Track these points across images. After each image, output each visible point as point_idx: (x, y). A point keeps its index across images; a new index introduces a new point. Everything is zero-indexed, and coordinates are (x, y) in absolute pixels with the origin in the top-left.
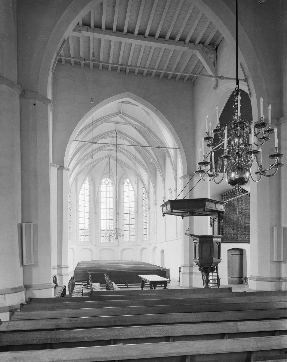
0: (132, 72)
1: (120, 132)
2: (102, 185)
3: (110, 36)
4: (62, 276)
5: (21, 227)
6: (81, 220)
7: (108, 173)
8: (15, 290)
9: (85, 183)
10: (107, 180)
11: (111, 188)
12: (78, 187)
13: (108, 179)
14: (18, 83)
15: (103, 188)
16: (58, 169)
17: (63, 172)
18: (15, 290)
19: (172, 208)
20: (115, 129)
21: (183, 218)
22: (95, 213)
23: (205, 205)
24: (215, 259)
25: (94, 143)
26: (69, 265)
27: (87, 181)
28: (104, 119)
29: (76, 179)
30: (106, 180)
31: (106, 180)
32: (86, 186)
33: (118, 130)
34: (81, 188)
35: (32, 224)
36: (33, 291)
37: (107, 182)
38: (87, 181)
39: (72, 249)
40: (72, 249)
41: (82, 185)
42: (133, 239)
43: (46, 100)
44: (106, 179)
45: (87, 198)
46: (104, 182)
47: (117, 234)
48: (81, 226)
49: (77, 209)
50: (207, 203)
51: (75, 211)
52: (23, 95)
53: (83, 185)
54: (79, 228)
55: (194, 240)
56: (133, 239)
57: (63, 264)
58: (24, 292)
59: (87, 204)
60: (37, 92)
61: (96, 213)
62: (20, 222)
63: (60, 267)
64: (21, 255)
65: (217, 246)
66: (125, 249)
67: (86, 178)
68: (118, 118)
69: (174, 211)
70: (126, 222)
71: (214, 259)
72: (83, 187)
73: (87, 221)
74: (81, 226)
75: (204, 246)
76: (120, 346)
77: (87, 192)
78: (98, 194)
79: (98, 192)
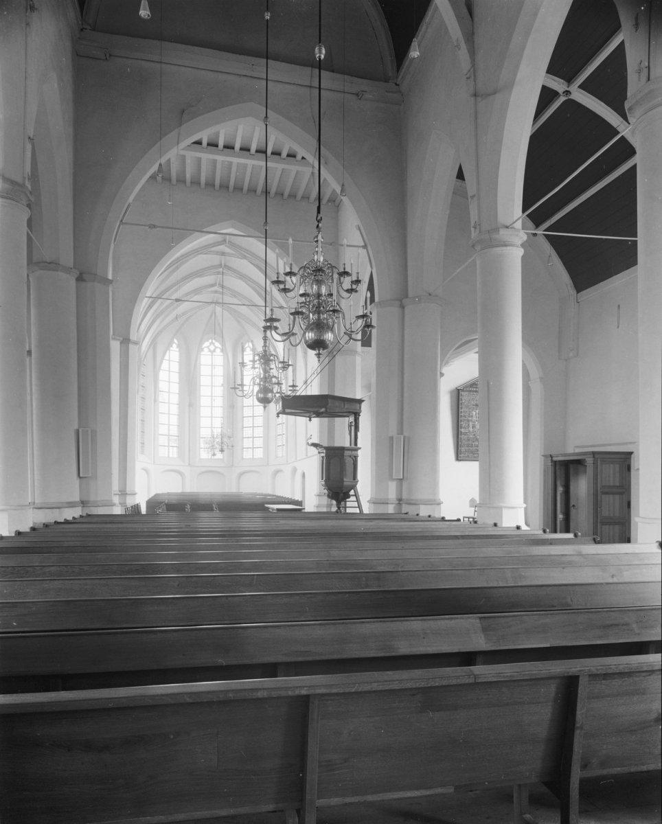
0: (238, 188)
1: (229, 268)
2: (202, 353)
5: (77, 432)
7: (215, 331)
8: (71, 505)
9: (171, 348)
10: (214, 344)
11: (219, 359)
12: (158, 359)
13: (214, 341)
14: (75, 268)
16: (121, 343)
18: (71, 505)
19: (284, 407)
21: (310, 420)
22: (190, 405)
24: (347, 481)
25: (177, 300)
26: (137, 490)
27: (174, 346)
28: (196, 252)
29: (154, 343)
30: (212, 343)
31: (212, 343)
32: (174, 354)
33: (225, 266)
34: (163, 359)
36: (92, 508)
37: (212, 348)
39: (146, 470)
40: (145, 470)
41: (164, 354)
42: (259, 454)
43: (107, 282)
44: (210, 341)
45: (175, 377)
48: (163, 430)
50: (330, 401)
52: (80, 279)
59: (175, 388)
62: (76, 427)
63: (123, 493)
66: (244, 473)
67: (172, 339)
68: (222, 248)
71: (345, 480)
72: (167, 357)
77: (175, 367)
79: (195, 365)
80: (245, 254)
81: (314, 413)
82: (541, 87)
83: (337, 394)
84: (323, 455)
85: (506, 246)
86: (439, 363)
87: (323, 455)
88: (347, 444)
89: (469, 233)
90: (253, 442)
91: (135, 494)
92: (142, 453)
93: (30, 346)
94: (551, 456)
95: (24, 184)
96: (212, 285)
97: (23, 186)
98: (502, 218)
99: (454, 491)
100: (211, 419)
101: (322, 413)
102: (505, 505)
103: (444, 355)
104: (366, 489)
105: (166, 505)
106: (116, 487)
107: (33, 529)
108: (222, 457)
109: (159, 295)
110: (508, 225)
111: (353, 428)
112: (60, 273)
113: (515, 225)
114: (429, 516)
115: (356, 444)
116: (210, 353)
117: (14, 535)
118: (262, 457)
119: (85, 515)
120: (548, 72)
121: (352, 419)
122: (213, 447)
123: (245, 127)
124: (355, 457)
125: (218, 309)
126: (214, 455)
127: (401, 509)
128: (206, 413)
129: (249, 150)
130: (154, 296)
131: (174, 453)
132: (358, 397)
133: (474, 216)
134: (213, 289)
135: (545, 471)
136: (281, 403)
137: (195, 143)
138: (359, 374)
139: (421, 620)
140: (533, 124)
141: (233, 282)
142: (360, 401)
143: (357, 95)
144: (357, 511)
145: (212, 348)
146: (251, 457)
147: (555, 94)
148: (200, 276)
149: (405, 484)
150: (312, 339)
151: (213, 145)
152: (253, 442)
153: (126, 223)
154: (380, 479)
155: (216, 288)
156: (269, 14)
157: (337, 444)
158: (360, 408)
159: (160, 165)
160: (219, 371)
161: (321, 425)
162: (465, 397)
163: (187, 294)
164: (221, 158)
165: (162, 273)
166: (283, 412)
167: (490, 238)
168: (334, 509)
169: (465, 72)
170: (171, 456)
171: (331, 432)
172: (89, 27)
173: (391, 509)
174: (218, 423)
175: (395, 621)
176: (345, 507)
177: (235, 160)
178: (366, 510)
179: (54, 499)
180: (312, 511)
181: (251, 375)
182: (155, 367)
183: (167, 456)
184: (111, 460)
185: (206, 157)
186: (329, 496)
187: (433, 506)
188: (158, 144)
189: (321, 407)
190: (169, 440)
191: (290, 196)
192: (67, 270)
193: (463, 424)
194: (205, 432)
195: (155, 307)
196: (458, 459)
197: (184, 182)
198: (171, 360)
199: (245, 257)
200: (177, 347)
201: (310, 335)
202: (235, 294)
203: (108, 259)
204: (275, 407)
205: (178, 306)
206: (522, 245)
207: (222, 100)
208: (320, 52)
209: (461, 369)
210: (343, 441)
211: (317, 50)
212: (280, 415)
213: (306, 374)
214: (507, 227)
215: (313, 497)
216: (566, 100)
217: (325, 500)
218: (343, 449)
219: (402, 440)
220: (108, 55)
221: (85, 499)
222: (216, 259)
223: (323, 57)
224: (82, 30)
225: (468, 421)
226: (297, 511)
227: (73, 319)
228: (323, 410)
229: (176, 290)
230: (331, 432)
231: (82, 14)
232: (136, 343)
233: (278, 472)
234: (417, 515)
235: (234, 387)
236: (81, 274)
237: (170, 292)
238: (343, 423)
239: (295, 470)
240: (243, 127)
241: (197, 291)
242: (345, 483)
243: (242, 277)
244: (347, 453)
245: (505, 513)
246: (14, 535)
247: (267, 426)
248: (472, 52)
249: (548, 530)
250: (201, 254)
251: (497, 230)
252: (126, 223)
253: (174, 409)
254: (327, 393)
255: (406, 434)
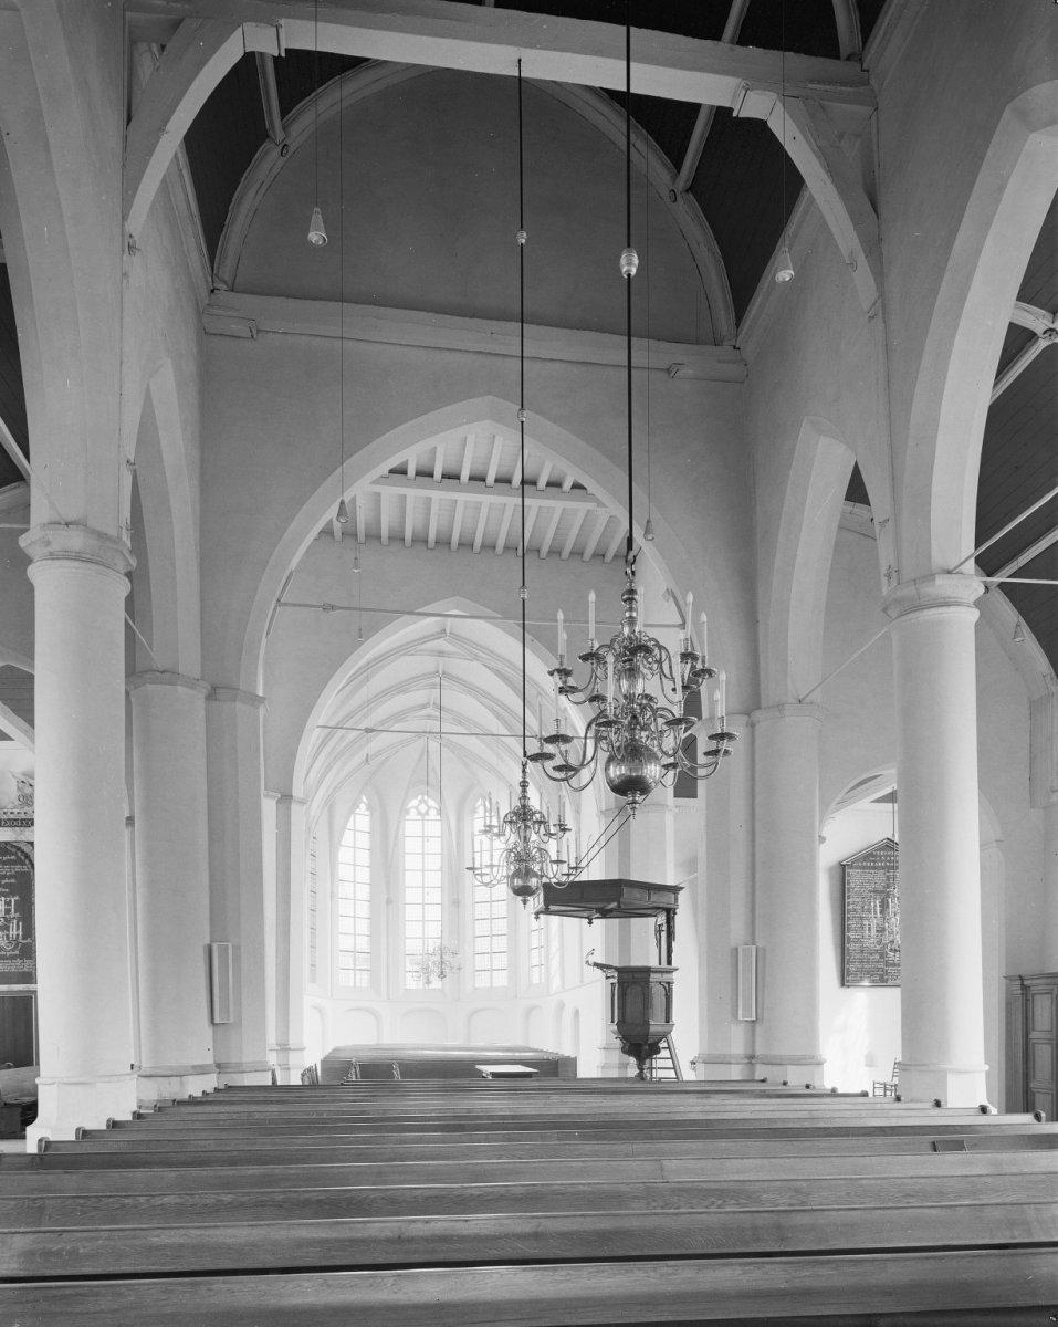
3: (404, 489)
4: (288, 1069)
6: (345, 925)
7: (428, 782)
8: (201, 1070)
10: (426, 803)
11: (434, 827)
13: (426, 798)
15: (411, 826)
17: (289, 809)
18: (201, 1070)
19: (547, 902)
20: (433, 670)
21: (590, 923)
23: (621, 894)
24: (656, 1025)
25: (368, 730)
27: (363, 806)
29: (330, 805)
32: (362, 820)
33: (444, 673)
34: (344, 828)
35: (230, 945)
38: (363, 806)
39: (319, 1009)
42: (501, 980)
43: (256, 701)
44: (420, 798)
45: (364, 858)
46: (416, 808)
47: (444, 964)
48: (345, 943)
49: (332, 892)
51: (329, 898)
52: (212, 695)
53: (352, 819)
54: (341, 948)
55: (607, 978)
56: (501, 980)
57: (292, 1042)
58: (215, 1075)
59: (364, 875)
60: (238, 689)
61: (391, 902)
62: (208, 942)
63: (284, 1048)
64: (209, 1004)
65: (664, 993)
69: (552, 908)
70: (482, 928)
71: (652, 1022)
72: (350, 825)
73: (363, 927)
74: (345, 943)
75: (629, 990)
76: (397, 1166)
77: (364, 840)
78: (395, 845)
79: (396, 837)
80: (475, 651)
81: (598, 910)
82: (1008, 324)
83: (635, 877)
84: (612, 981)
85: (947, 604)
86: (817, 818)
87: (612, 981)
88: (653, 962)
89: (877, 591)
90: (491, 961)
91: (304, 1049)
92: (313, 980)
93: (132, 810)
94: (1021, 978)
95: (120, 538)
96: (424, 707)
97: (117, 540)
98: (938, 558)
99: (850, 1045)
100: (422, 926)
101: (611, 910)
102: (950, 1067)
103: (825, 805)
104: (688, 1039)
105: (362, 1067)
106: (272, 1038)
107: (138, 1116)
108: (440, 986)
109: (338, 724)
110: (951, 568)
111: (664, 935)
112: (180, 688)
113: (963, 568)
114: (808, 1087)
115: (669, 962)
116: (419, 817)
117: (105, 1128)
118: (506, 984)
119: (222, 1087)
120: (1021, 298)
121: (662, 919)
122: (426, 969)
123: (467, 446)
124: (669, 983)
125: (434, 745)
126: (428, 982)
127: (753, 1072)
128: (411, 916)
129: (483, 480)
130: (332, 724)
131: (363, 980)
132: (670, 882)
133: (886, 557)
134: (424, 712)
135: (1008, 1004)
136: (542, 895)
137: (391, 471)
138: (668, 841)
139: (785, 1263)
140: (995, 385)
141: (456, 699)
142: (675, 890)
143: (668, 371)
144: (672, 1074)
145: (423, 808)
146: (489, 985)
147: (1031, 336)
148: (404, 692)
149: (759, 1029)
150: (621, 776)
151: (425, 473)
152: (491, 961)
153: (286, 604)
154: (713, 1023)
155: (428, 711)
156: (525, 235)
157: (636, 962)
158: (676, 899)
159: (342, 503)
160: (435, 846)
161: (607, 930)
162: (856, 878)
163: (382, 722)
164: (439, 496)
165: (343, 687)
166: (547, 911)
167: (913, 598)
168: (633, 1072)
169: (866, 305)
170: (358, 985)
171: (625, 942)
172: (225, 287)
173: (735, 1072)
174: (434, 930)
175: (732, 1264)
176: (651, 1069)
177: (462, 497)
178: (688, 1075)
179: (173, 1060)
180: (595, 1076)
181: (493, 852)
182: (331, 837)
183: (352, 985)
184: (264, 997)
185: (414, 494)
186: (624, 1051)
187: (810, 1067)
188: (339, 470)
189: (610, 902)
190: (355, 960)
191: (550, 552)
192: (192, 683)
193: (852, 923)
194: (413, 946)
195: (331, 744)
196: (843, 985)
197: (379, 537)
198: (359, 826)
199: (477, 658)
200: (367, 809)
201: (617, 771)
202: (459, 719)
203: (256, 676)
204: (536, 902)
205: (368, 741)
206: (978, 604)
207: (441, 392)
208: (630, 264)
209: (852, 828)
210: (646, 954)
211: (623, 260)
212: (541, 916)
213: (585, 841)
214: (949, 572)
215: (593, 1050)
216: (1048, 346)
217: (617, 1056)
218: (647, 971)
219: (754, 954)
220: (254, 332)
221: (223, 1060)
222: (429, 664)
223: (634, 271)
224: (212, 291)
225: (861, 918)
226: (553, 1070)
227: (201, 763)
228: (613, 905)
229: (365, 716)
230: (625, 942)
231: (213, 268)
232: (302, 802)
233: (530, 1010)
234: (785, 1083)
235: (459, 870)
236: (214, 688)
237: (357, 717)
238: (645, 929)
239: (561, 1006)
240: (477, 437)
241: (399, 716)
242: (652, 1029)
243: (470, 689)
244: (654, 977)
245: (952, 1080)
246: (105, 1128)
247: (513, 933)
248: (879, 274)
249: (1043, 1115)
250: (404, 654)
251: (929, 577)
252: (286, 604)
253: (364, 910)
254: (616, 877)
255: (760, 943)
